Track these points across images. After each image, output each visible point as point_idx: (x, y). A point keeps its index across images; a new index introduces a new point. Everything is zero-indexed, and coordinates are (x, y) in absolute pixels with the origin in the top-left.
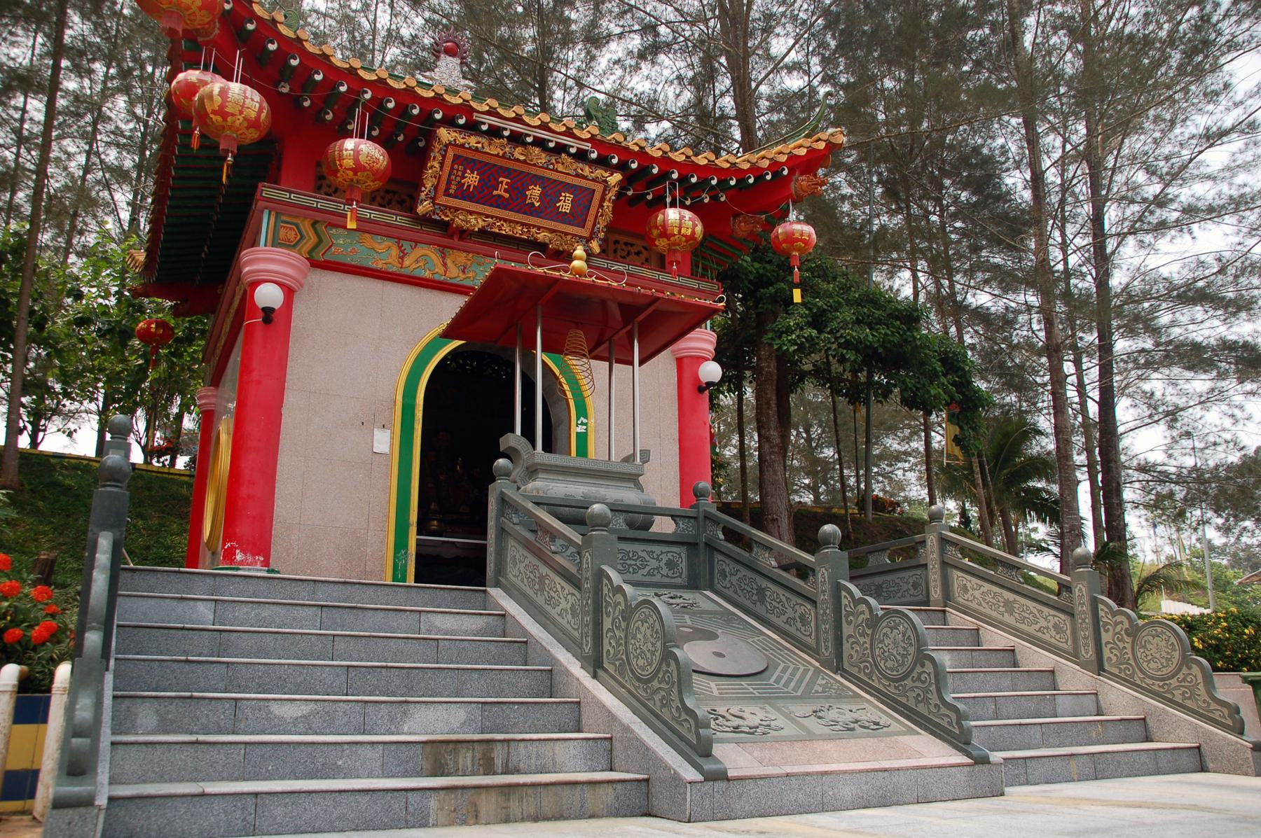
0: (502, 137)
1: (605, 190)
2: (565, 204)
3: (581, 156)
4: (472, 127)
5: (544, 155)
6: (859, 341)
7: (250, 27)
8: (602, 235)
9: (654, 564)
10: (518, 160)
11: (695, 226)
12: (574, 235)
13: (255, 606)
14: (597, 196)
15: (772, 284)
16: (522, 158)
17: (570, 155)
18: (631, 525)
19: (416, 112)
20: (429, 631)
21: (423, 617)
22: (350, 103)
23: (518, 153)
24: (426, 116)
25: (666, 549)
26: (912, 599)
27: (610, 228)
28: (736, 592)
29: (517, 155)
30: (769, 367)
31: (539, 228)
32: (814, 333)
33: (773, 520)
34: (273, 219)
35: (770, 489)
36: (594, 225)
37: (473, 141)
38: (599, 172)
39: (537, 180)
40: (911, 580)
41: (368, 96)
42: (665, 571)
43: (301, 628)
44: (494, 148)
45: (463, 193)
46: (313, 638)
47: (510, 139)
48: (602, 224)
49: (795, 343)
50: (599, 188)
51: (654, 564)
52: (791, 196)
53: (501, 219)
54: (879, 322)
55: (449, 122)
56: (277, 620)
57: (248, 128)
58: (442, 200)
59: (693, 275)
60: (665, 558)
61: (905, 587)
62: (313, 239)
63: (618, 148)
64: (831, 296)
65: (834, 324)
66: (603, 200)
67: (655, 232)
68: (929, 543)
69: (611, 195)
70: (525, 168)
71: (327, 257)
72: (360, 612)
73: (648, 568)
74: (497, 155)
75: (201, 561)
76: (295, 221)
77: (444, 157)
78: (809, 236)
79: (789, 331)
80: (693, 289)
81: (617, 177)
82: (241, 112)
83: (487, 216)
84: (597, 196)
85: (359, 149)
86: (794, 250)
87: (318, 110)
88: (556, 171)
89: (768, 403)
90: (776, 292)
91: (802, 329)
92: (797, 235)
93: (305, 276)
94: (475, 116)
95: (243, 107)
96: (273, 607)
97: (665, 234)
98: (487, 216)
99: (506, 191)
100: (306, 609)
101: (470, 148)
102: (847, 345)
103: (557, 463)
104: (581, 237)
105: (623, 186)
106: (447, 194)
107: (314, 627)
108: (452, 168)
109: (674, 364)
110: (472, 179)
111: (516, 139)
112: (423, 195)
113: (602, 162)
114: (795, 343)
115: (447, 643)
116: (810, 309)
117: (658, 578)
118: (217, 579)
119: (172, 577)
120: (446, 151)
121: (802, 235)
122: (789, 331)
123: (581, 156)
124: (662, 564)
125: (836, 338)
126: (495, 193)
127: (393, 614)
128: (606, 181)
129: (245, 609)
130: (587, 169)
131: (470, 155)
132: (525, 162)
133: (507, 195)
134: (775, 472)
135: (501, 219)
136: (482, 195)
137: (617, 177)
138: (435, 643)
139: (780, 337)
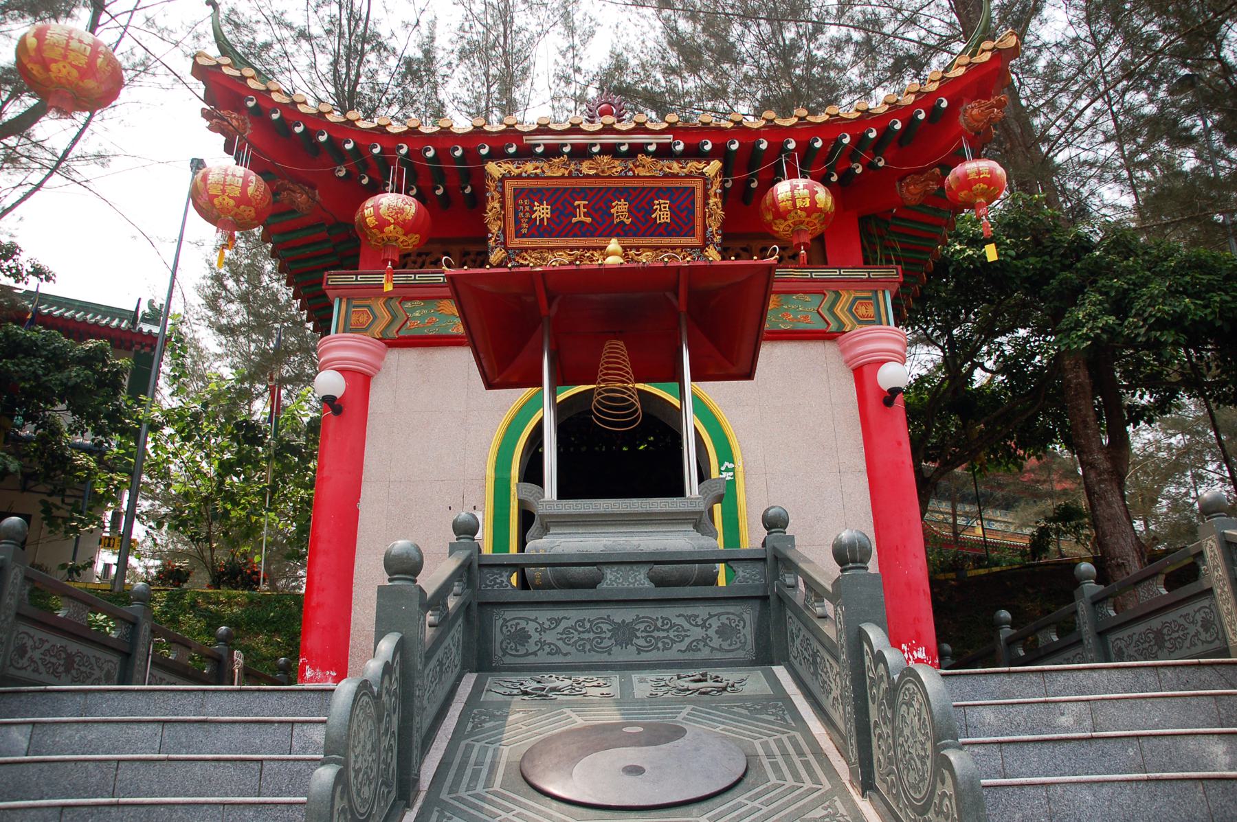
0: (561, 154)
1: (705, 184)
2: (662, 212)
3: (664, 152)
4: (526, 153)
5: (617, 163)
6: (1183, 315)
7: (275, 116)
8: (718, 239)
9: (698, 632)
10: (588, 176)
11: (813, 193)
12: (683, 248)
13: (81, 727)
14: (699, 194)
15: (1053, 276)
16: (592, 172)
17: (648, 153)
18: (660, 582)
19: (458, 153)
20: (304, 750)
21: (297, 730)
22: (385, 162)
23: (586, 168)
24: (471, 155)
25: (717, 610)
26: (1207, 647)
27: (725, 226)
28: (98, 659)
29: (585, 171)
30: (1077, 377)
31: (638, 248)
32: (1111, 320)
33: (1119, 566)
34: (344, 306)
35: (1107, 526)
36: (705, 228)
37: (529, 167)
38: (693, 165)
39: (620, 193)
40: (1199, 617)
41: (404, 151)
42: (716, 642)
43: (135, 752)
44: (555, 169)
45: (538, 230)
46: (91, 766)
47: (571, 155)
48: (714, 226)
49: (1087, 338)
50: (698, 185)
51: (698, 632)
52: (962, 132)
53: (589, 249)
54: (1210, 288)
55: (498, 154)
56: (107, 743)
57: (238, 206)
58: (515, 243)
59: (867, 262)
60: (715, 624)
61: (1192, 630)
62: (387, 317)
63: (706, 130)
64: (1135, 271)
65: (1137, 305)
66: (706, 197)
67: (769, 217)
68: (1208, 553)
69: (716, 188)
70: (599, 184)
71: (403, 333)
72: (212, 728)
73: (687, 641)
74: (563, 177)
75: (137, 676)
76: (368, 302)
77: (503, 194)
78: (991, 172)
79: (1078, 324)
80: (862, 281)
81: (714, 166)
82: (224, 191)
83: (572, 249)
84: (699, 194)
85: (393, 204)
86: (976, 196)
87: (352, 177)
88: (639, 177)
89: (1084, 421)
90: (1060, 284)
91: (1095, 319)
92: (972, 176)
93: (382, 358)
94: (527, 140)
95: (224, 185)
96: (103, 727)
97: (780, 214)
98: (572, 249)
99: (585, 215)
100: (143, 727)
101: (529, 177)
102: (1161, 324)
103: (572, 511)
104: (692, 248)
105: (724, 172)
106: (519, 235)
107: (152, 750)
108: (516, 205)
109: (851, 376)
110: (543, 211)
111: (581, 153)
112: (491, 243)
113: (693, 152)
114: (1087, 338)
115: (276, 765)
116: (1107, 294)
117: (705, 653)
118: (89, 696)
119: (38, 697)
120: (503, 187)
121: (979, 173)
122: (1078, 324)
123: (664, 152)
124: (711, 632)
125: (1145, 320)
126: (574, 220)
127: (256, 727)
128: (703, 174)
129: (68, 731)
130: (675, 165)
131: (532, 184)
132: (597, 176)
133: (588, 220)
134: (1109, 505)
135: (589, 249)
136: (560, 226)
137: (714, 166)
138: (257, 766)
139: (1068, 336)
